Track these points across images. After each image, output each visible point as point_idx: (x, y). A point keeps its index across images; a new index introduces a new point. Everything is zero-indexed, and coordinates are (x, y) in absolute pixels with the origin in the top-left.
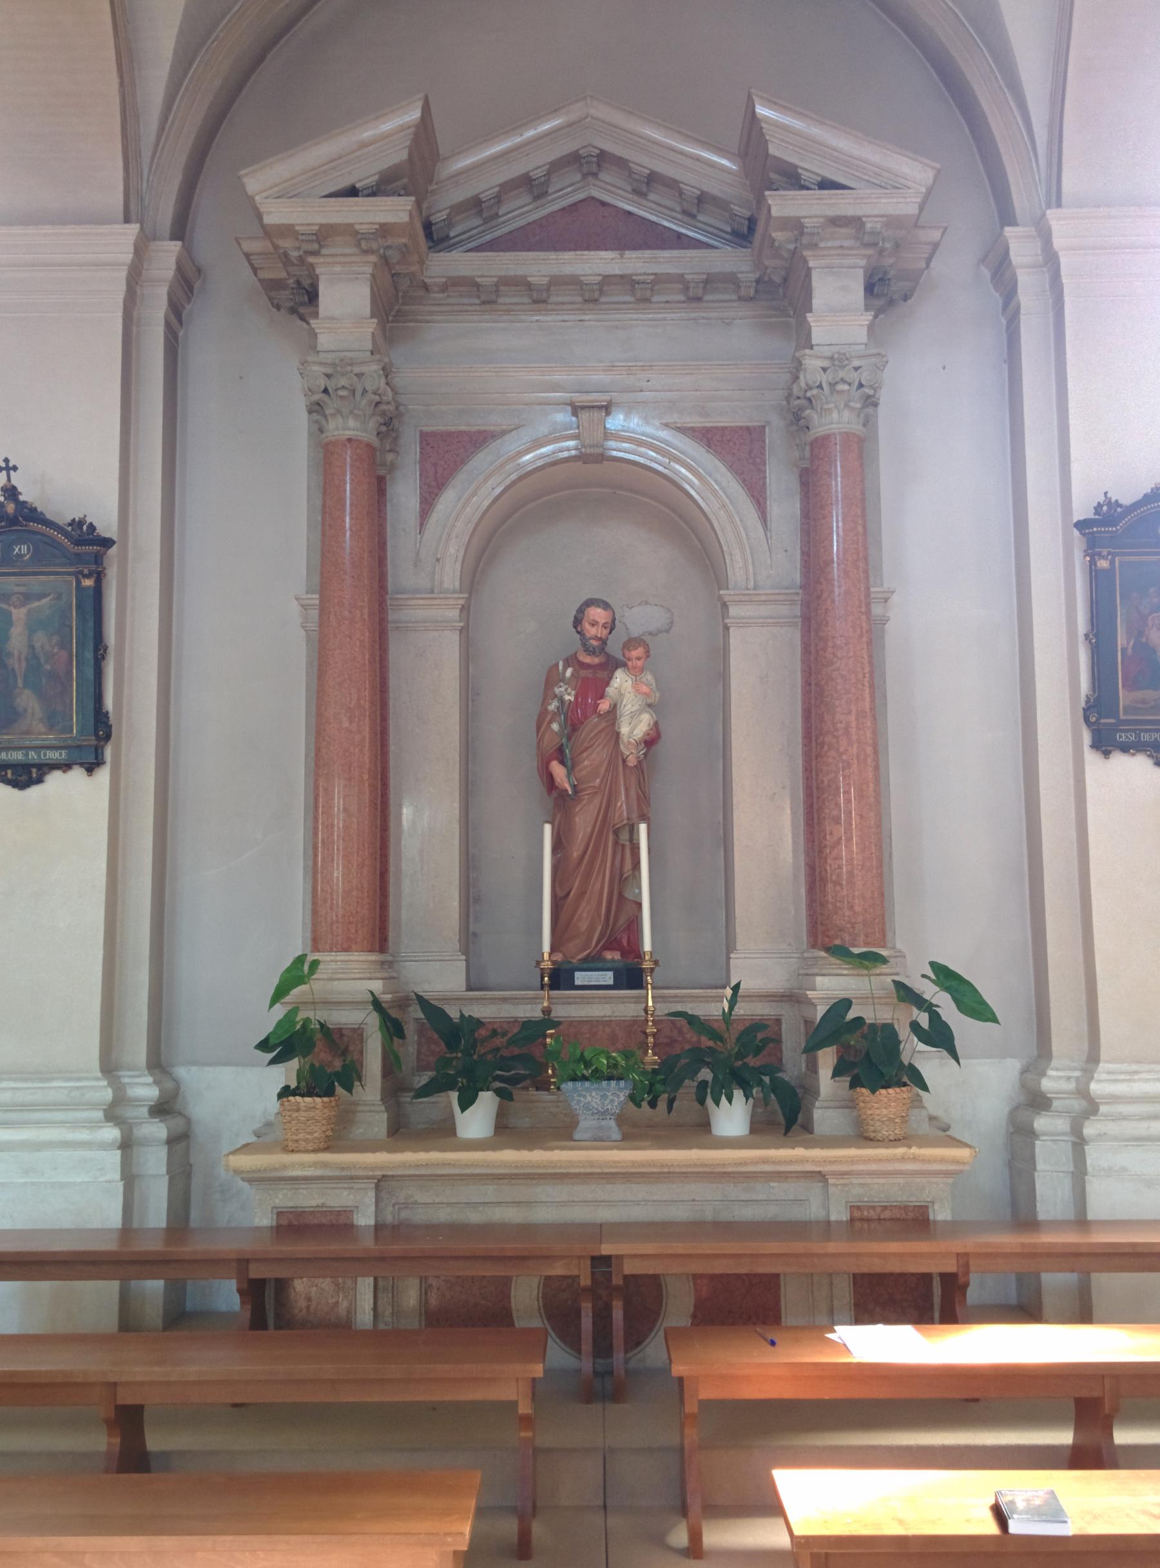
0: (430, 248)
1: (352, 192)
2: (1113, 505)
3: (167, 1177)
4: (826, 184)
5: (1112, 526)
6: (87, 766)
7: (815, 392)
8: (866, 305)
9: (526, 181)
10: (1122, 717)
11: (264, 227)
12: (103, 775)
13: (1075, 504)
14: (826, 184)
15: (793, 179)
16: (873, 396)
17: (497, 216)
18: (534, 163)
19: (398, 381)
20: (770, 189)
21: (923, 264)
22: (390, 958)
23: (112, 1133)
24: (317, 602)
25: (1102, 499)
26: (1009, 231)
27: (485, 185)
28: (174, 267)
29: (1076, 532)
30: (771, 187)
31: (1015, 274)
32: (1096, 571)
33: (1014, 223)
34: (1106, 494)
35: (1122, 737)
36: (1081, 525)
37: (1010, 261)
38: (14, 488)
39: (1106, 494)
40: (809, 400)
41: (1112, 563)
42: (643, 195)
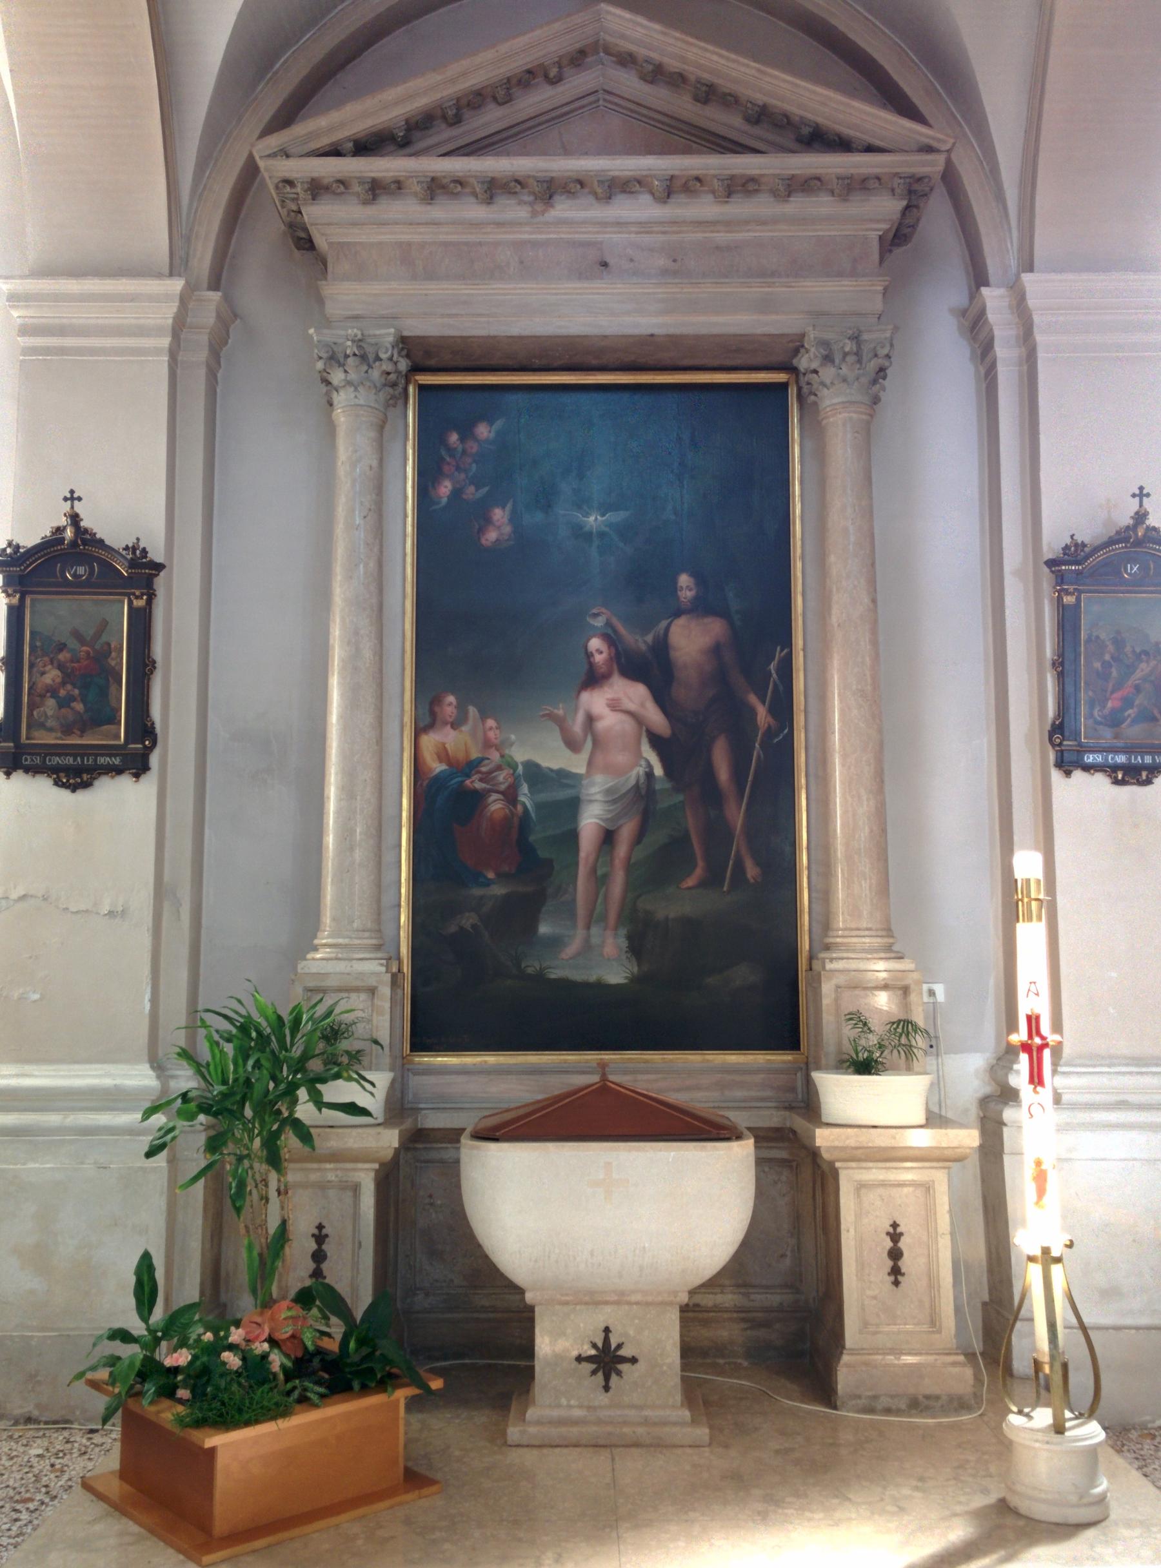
25: (1068, 541)
26: (985, 291)
28: (214, 315)
29: (1046, 570)
31: (991, 330)
33: (987, 284)
34: (1072, 537)
35: (1090, 759)
36: (1051, 563)
37: (987, 318)
41: (1078, 599)
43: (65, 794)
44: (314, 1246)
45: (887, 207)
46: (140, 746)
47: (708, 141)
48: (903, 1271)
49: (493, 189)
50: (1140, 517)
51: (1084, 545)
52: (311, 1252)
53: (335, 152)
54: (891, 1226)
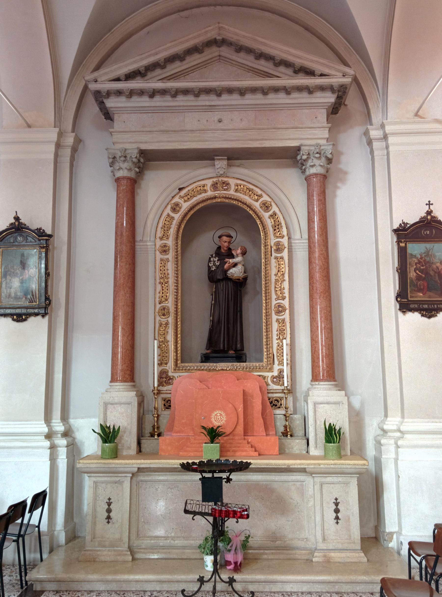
2: (406, 224)
3: (66, 459)
6: (42, 315)
12: (47, 318)
13: (394, 224)
23: (47, 443)
32: (400, 247)
35: (412, 306)
38: (18, 217)
39: (403, 220)
41: (406, 244)
43: (425, 319)
44: (107, 507)
45: (330, 98)
46: (406, 300)
47: (263, 74)
48: (111, 517)
49: (176, 93)
50: (429, 213)
51: (407, 224)
52: (106, 509)
53: (118, 79)
54: (108, 499)
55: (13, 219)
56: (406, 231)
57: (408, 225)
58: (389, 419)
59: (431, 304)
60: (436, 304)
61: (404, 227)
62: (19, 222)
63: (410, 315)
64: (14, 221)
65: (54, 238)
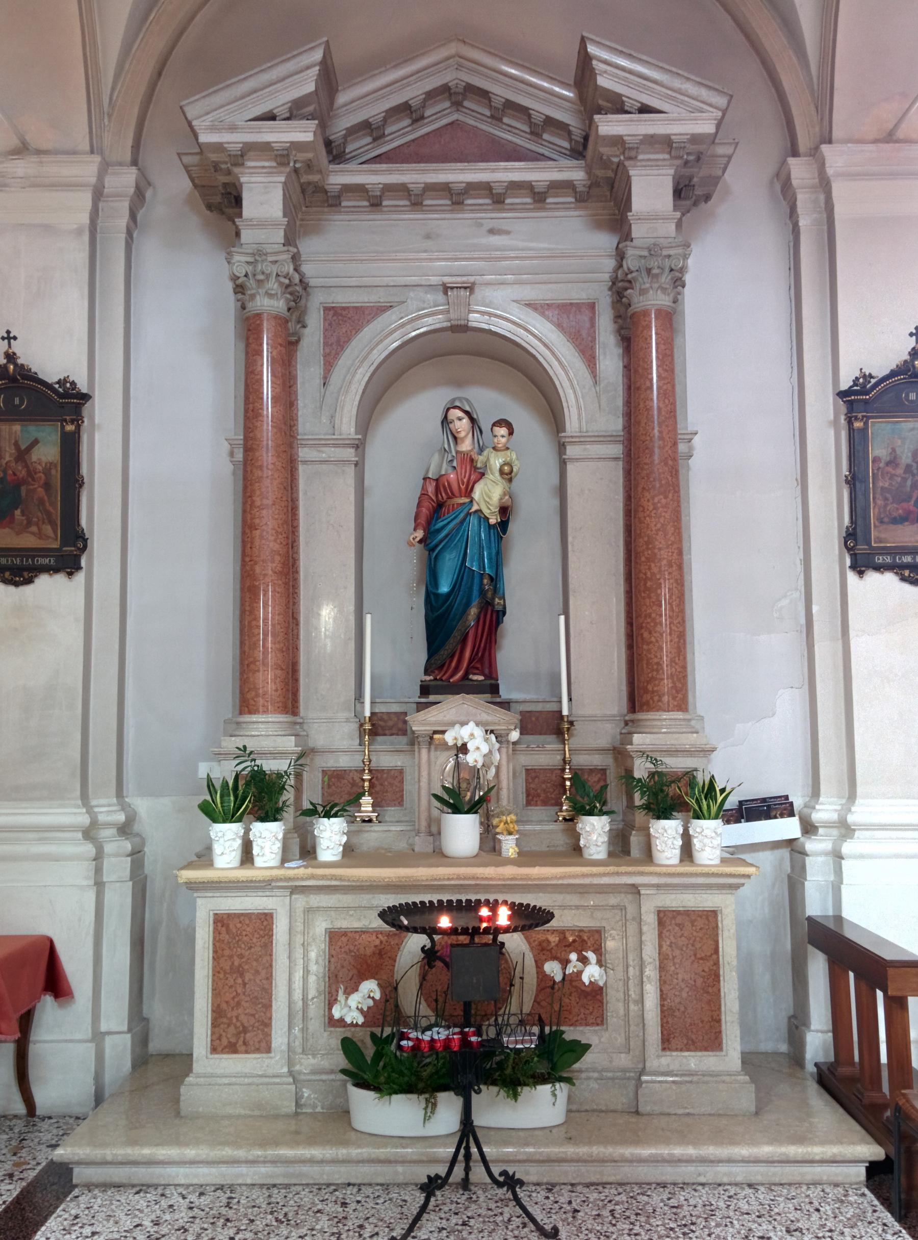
0: (330, 162)
1: (271, 117)
2: (868, 377)
4: (645, 109)
5: (866, 395)
7: (634, 274)
8: (675, 206)
9: (404, 109)
10: (873, 545)
11: (199, 145)
12: (80, 577)
14: (645, 109)
15: (618, 105)
16: (681, 279)
17: (383, 135)
18: (413, 93)
19: (306, 268)
20: (600, 113)
21: (720, 173)
22: (301, 721)
23: (89, 849)
24: (242, 442)
25: (857, 374)
27: (374, 111)
30: (599, 110)
35: (879, 560)
36: (842, 394)
40: (630, 282)
41: (866, 424)
42: (539, 136)
51: (871, 376)
55: (3, 356)
56: (867, 393)
57: (873, 381)
58: (858, 801)
59: (28, 557)
60: (10, 556)
61: (864, 386)
62: (16, 365)
63: (873, 577)
64: (5, 361)
65: (94, 401)
